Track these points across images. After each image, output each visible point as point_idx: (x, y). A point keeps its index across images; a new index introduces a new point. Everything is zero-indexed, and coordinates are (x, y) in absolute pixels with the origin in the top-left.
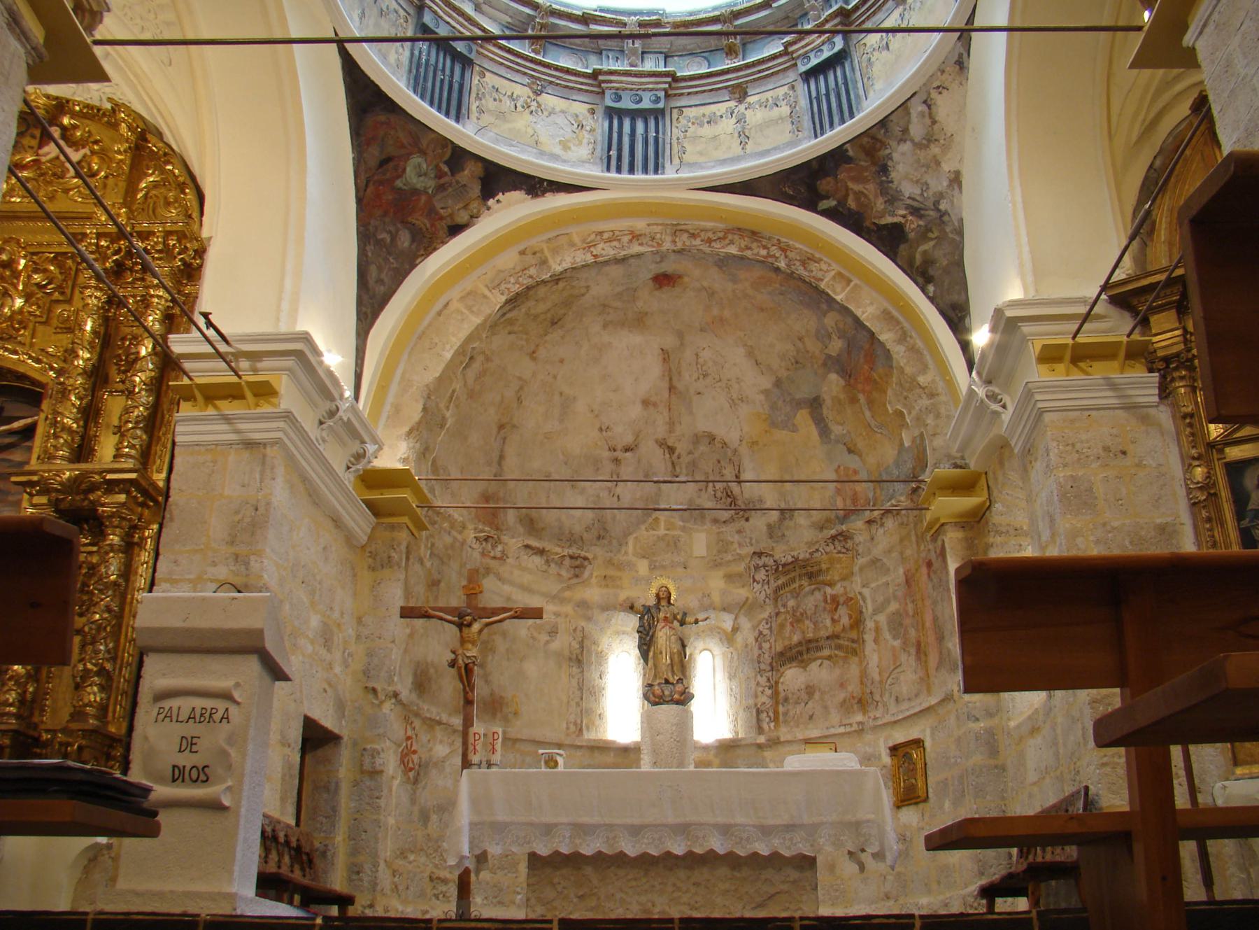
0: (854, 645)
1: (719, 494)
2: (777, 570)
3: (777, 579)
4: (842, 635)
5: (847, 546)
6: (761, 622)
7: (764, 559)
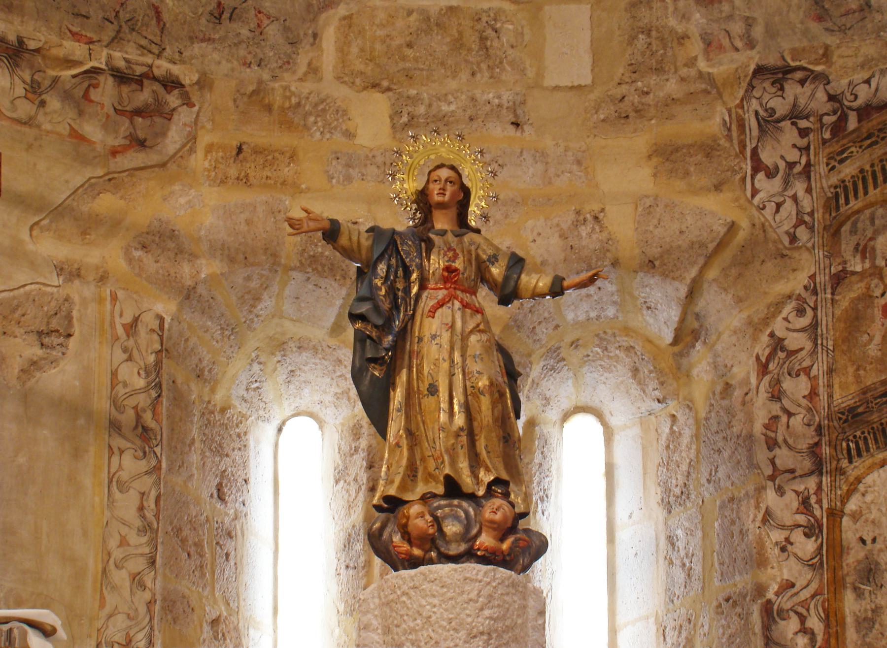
2: (838, 128)
3: (838, 159)
6: (778, 306)
7: (792, 89)
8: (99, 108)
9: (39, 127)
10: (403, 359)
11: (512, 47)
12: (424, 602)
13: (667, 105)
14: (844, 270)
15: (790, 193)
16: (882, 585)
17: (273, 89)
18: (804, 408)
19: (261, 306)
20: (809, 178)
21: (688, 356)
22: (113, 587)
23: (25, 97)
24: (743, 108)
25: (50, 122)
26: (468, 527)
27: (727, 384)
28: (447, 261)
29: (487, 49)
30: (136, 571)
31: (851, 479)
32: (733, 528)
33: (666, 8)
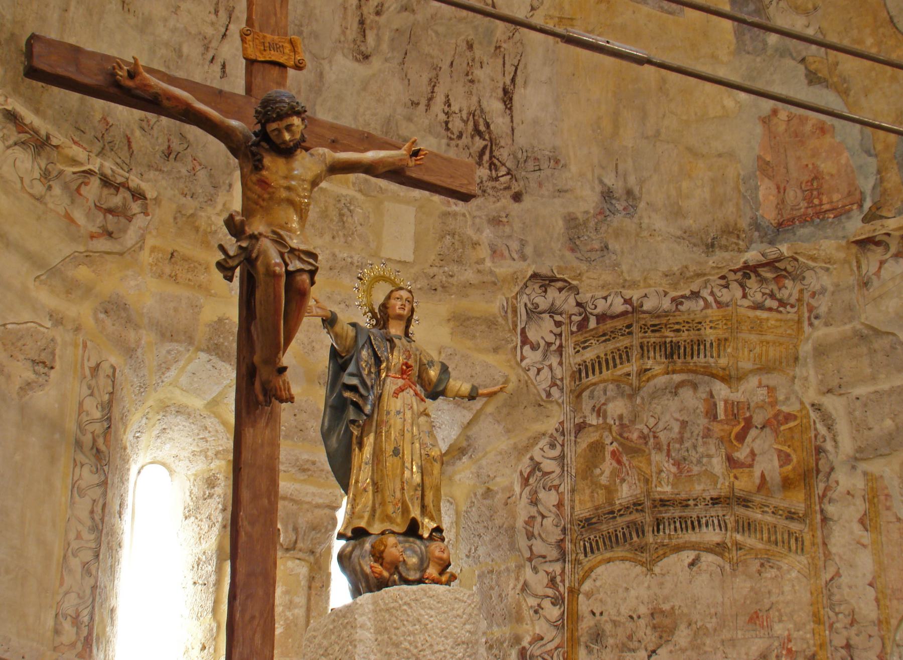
0: (795, 526)
1: (456, 124)
2: (583, 325)
3: (582, 346)
4: (758, 499)
5: (784, 294)
6: (535, 440)
7: (552, 293)
8: (85, 201)
9: (46, 204)
10: (371, 425)
11: (361, 225)
12: (422, 612)
13: (465, 287)
14: (584, 422)
15: (548, 363)
16: (606, 647)
17: (201, 216)
18: (554, 514)
19: (167, 374)
20: (561, 355)
21: (453, 465)
22: (70, 570)
23: (40, 180)
24: (517, 299)
25: (53, 203)
26: (422, 560)
27: (488, 489)
28: (405, 359)
29: (344, 223)
30: (86, 561)
31: (586, 568)
32: (492, 592)
33: (466, 222)
